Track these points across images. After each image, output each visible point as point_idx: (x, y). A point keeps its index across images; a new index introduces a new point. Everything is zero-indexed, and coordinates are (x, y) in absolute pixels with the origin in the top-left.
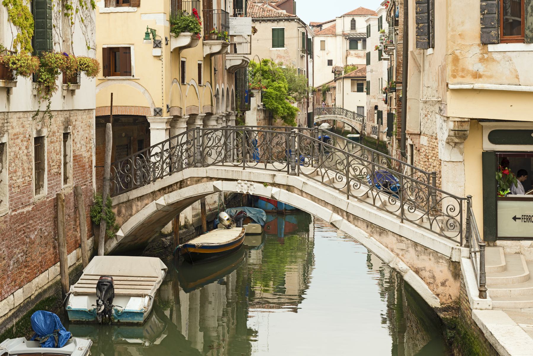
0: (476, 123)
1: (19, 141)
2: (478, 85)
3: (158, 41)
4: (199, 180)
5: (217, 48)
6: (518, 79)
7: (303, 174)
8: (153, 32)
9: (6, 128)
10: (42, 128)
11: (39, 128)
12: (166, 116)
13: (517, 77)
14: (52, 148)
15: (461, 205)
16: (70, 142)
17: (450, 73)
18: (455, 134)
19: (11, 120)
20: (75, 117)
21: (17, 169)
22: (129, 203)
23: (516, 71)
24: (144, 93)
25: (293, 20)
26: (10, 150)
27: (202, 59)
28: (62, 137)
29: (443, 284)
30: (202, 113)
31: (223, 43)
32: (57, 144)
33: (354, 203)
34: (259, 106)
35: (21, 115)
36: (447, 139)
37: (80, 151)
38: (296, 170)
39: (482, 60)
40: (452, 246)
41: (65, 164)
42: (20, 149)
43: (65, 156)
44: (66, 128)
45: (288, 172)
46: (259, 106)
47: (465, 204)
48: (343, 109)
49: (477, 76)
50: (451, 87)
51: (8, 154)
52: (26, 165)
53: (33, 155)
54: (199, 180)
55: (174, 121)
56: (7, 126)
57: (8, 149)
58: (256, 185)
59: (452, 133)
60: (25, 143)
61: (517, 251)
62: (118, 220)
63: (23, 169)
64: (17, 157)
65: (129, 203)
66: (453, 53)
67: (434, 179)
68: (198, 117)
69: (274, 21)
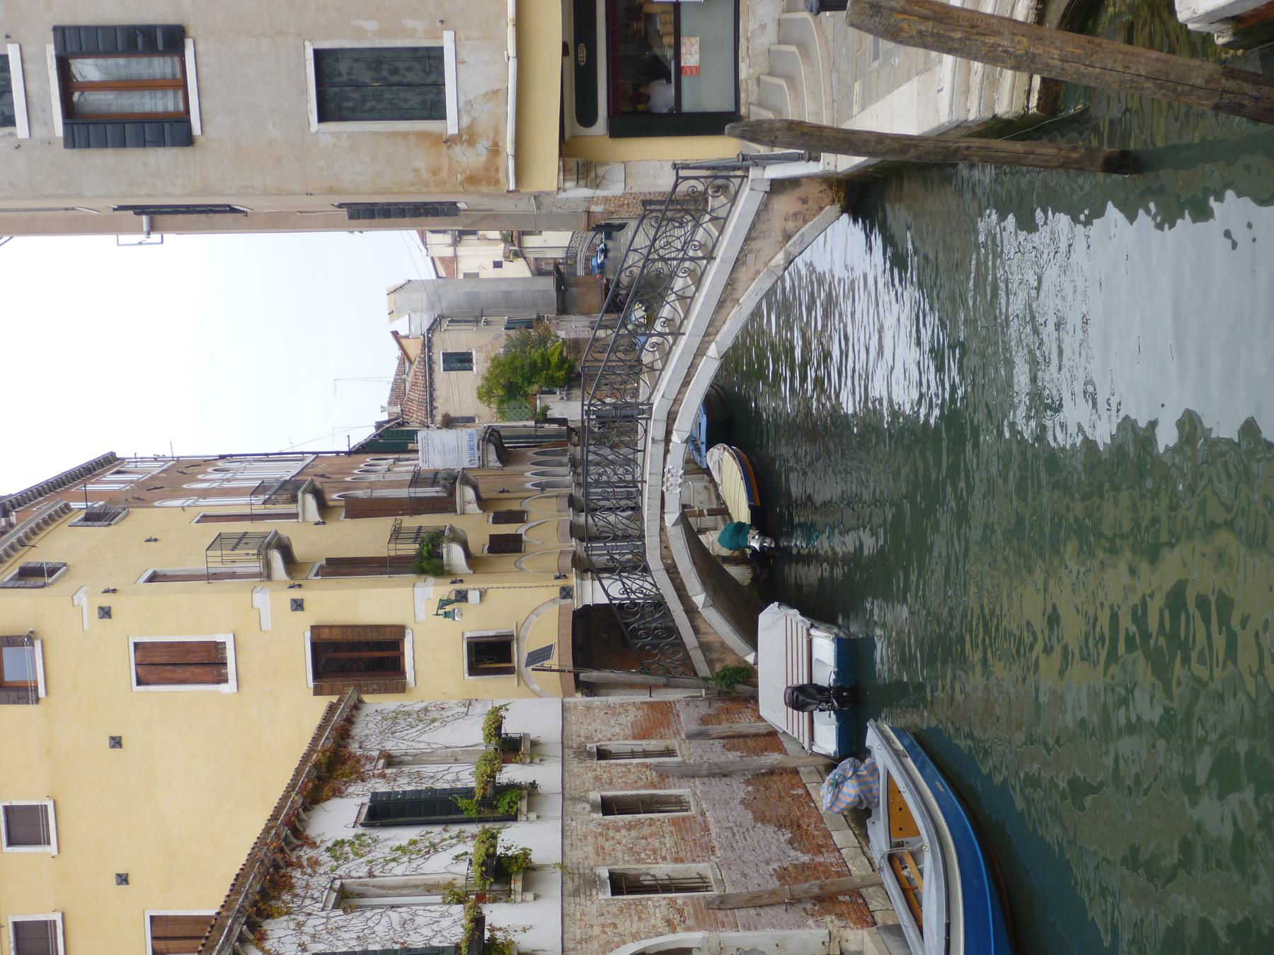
0: (566, 147)
1: (607, 845)
2: (510, 148)
3: (456, 596)
4: (665, 546)
5: (469, 493)
6: (498, 90)
7: (649, 398)
8: (443, 603)
9: (587, 871)
10: (588, 802)
11: (588, 807)
12: (573, 580)
13: (496, 92)
14: (620, 781)
15: (686, 178)
16: (612, 746)
17: (492, 187)
18: (583, 178)
19: (575, 860)
20: (574, 737)
21: (650, 847)
22: (705, 647)
23: (486, 95)
24: (538, 615)
25: (429, 340)
26: (621, 861)
27: (486, 515)
28: (603, 762)
29: (805, 201)
30: (569, 515)
31: (461, 483)
32: (613, 771)
33: (690, 327)
34: (562, 399)
35: (567, 842)
36: (591, 188)
37: (626, 726)
38: (645, 407)
39: (471, 142)
40: (748, 189)
41: (646, 754)
42: (619, 843)
43: (633, 754)
44: (590, 755)
45: (647, 419)
46: (562, 399)
47: (682, 173)
48: (569, 247)
49: (495, 150)
50: (512, 187)
51: (626, 866)
52: (646, 831)
53: (629, 817)
54: (665, 546)
55: (584, 567)
56: (584, 868)
57: (620, 867)
58: (669, 466)
59: (582, 182)
60: (611, 833)
61: (755, 83)
62: (730, 662)
63: (651, 835)
64: (631, 849)
65: (705, 647)
66: (461, 183)
67: (651, 202)
68: (575, 521)
69: (431, 369)
